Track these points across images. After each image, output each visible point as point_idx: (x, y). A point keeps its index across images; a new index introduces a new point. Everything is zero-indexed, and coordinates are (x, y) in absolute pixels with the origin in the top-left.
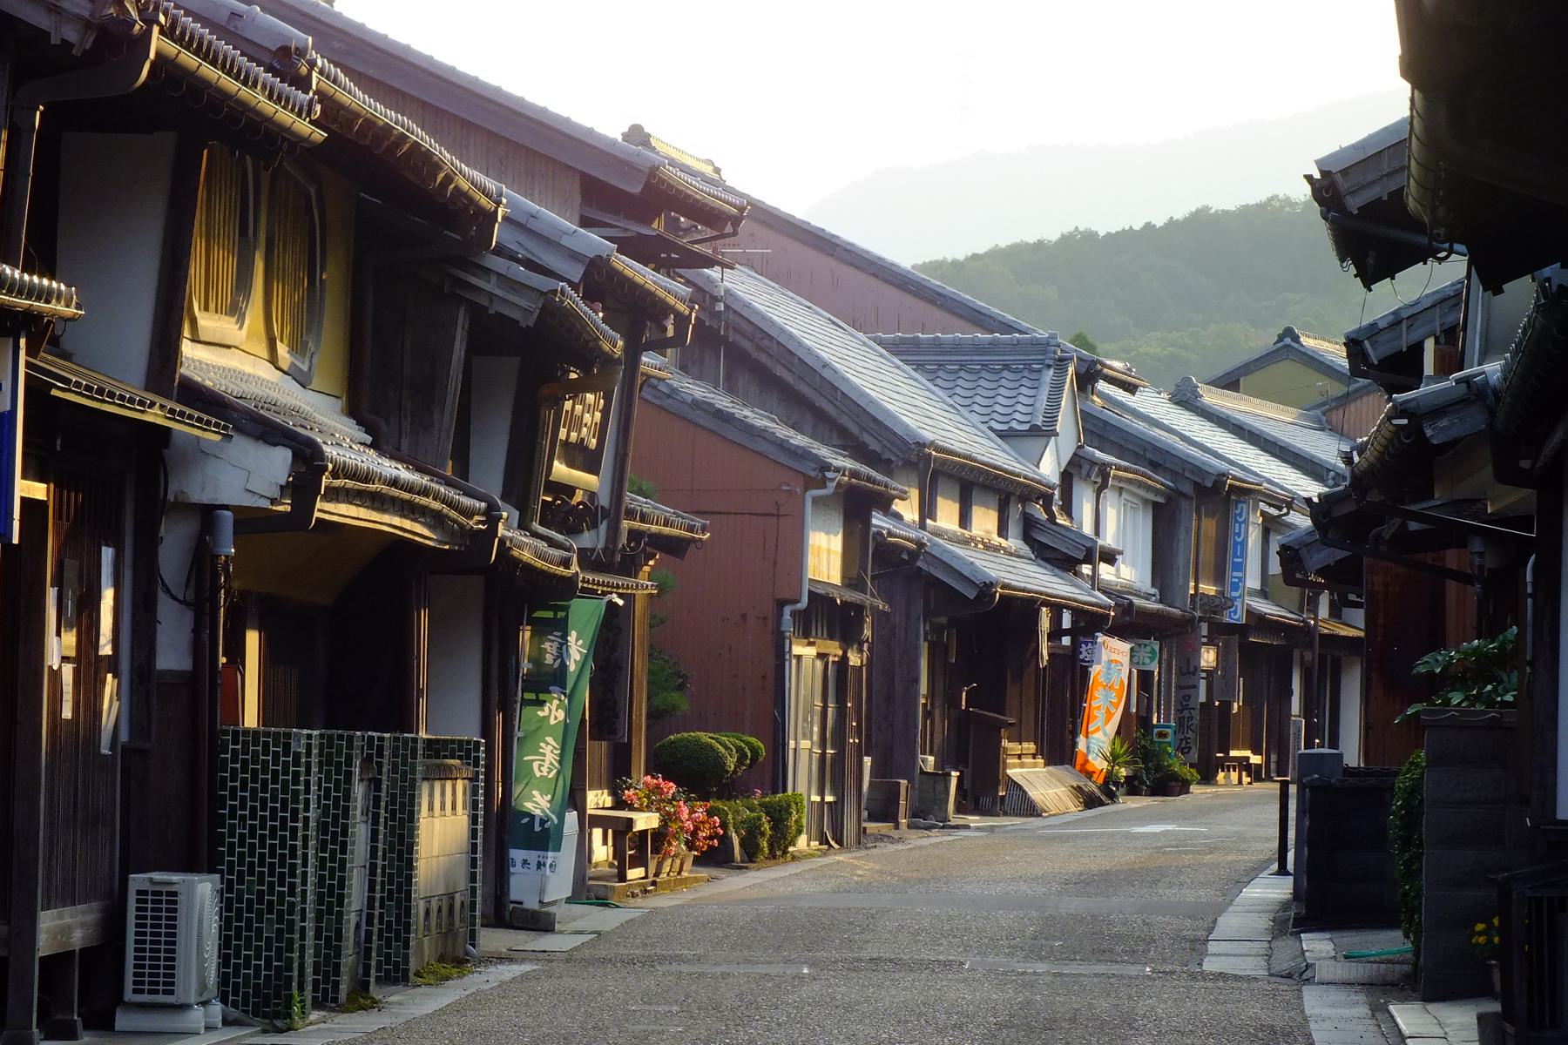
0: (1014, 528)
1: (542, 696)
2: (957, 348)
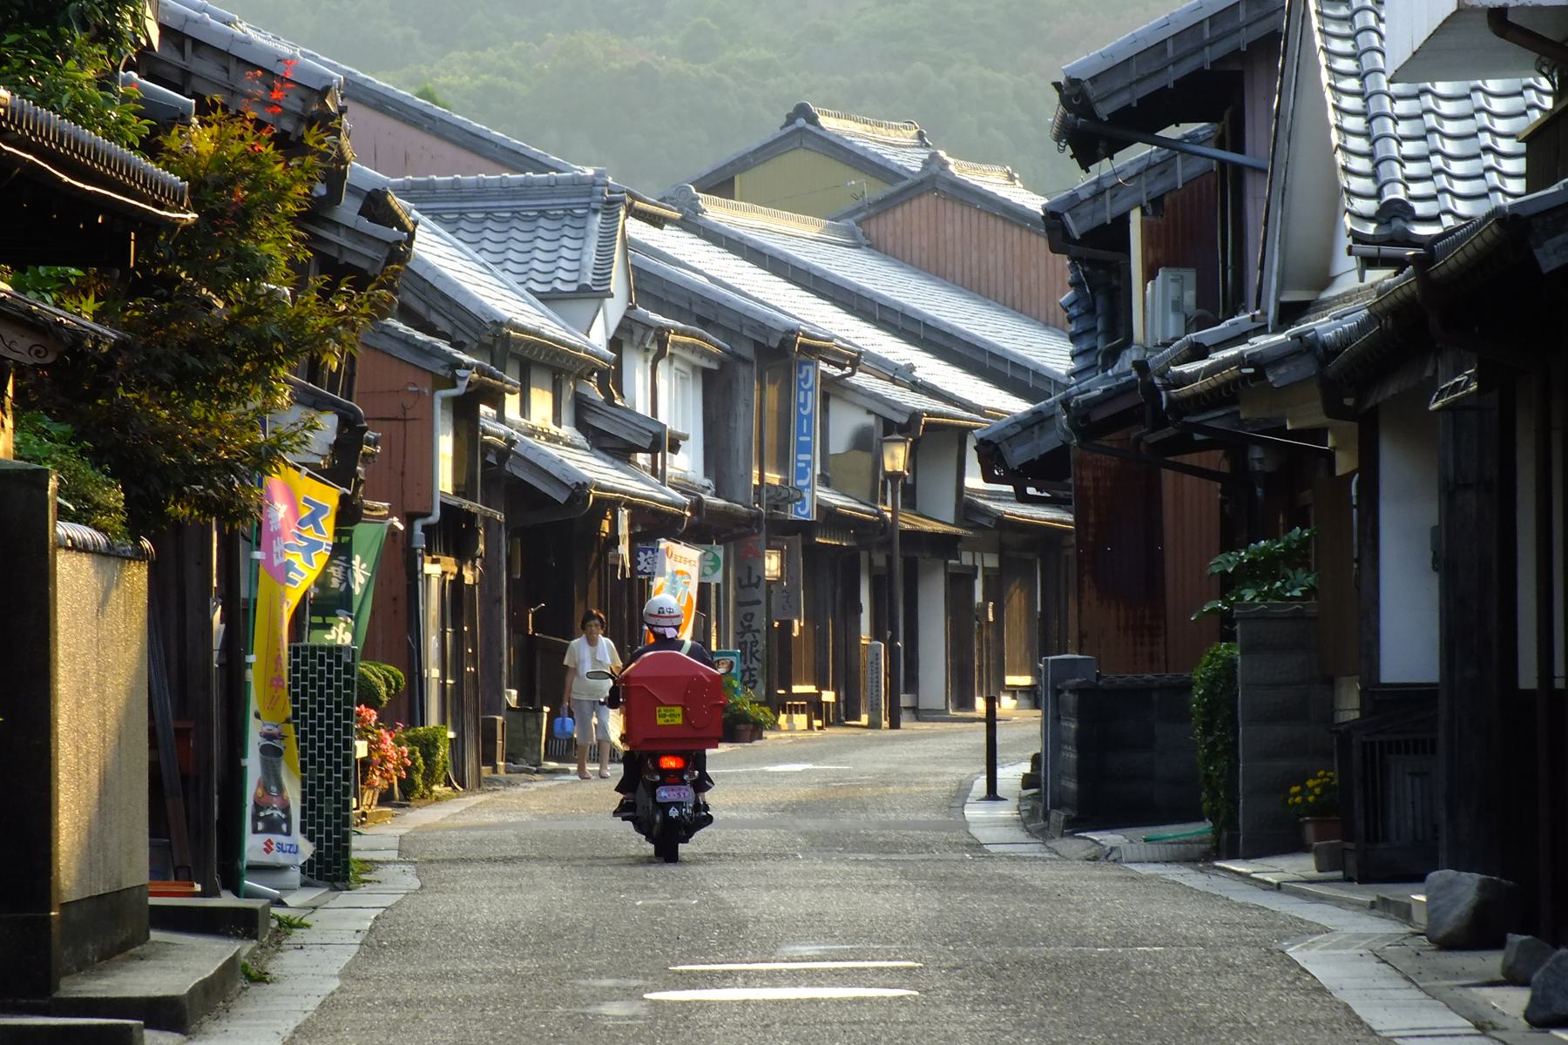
0: (567, 414)
1: (329, 620)
2: (481, 192)
